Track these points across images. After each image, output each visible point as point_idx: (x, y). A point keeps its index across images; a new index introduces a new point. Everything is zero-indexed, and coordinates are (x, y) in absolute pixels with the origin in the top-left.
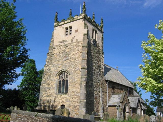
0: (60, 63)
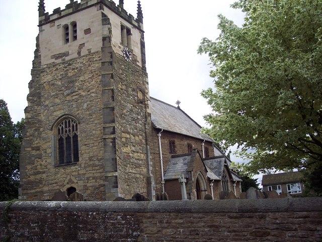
0: (57, 101)
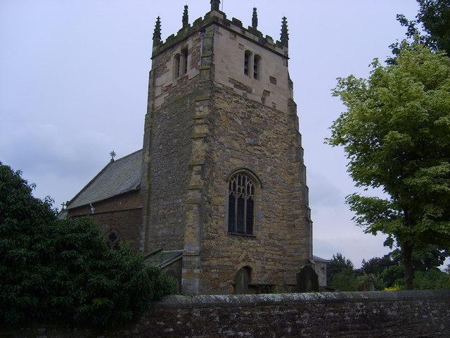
0: (236, 144)
